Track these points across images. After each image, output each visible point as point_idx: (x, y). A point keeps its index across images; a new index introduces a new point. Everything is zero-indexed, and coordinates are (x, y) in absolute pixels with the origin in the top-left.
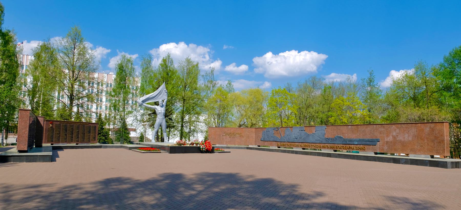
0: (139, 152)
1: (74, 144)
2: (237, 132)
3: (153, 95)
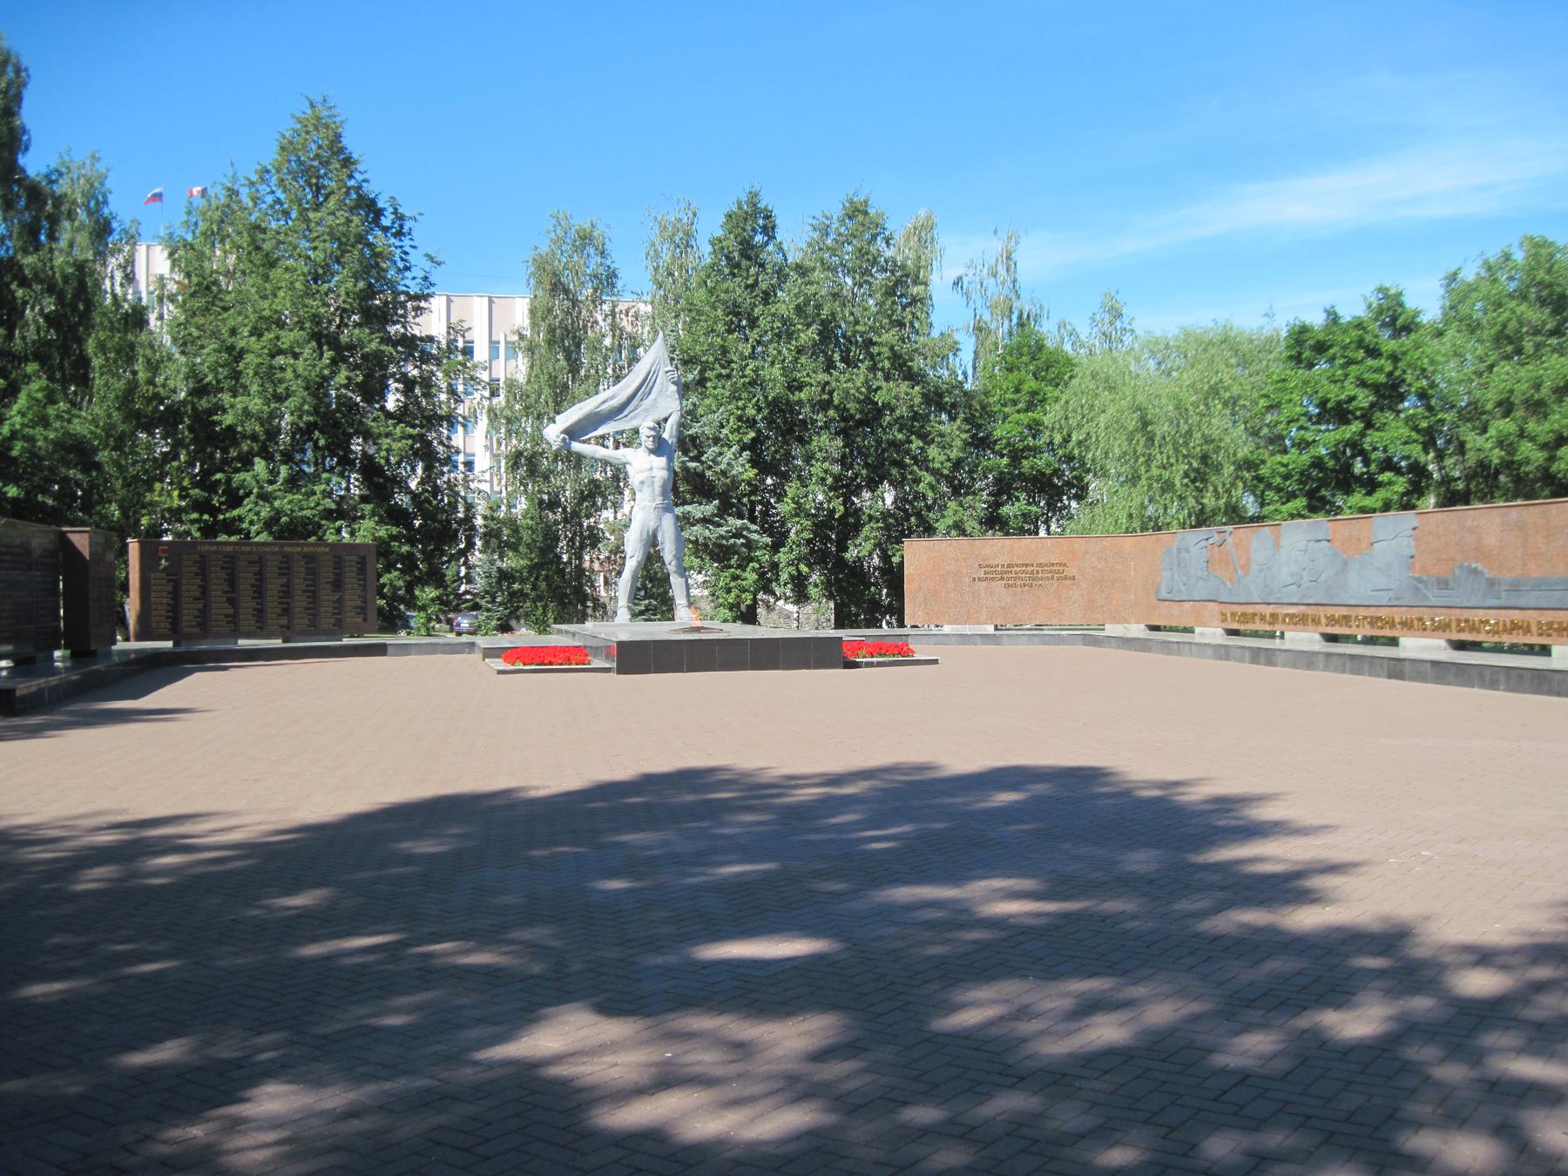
0: (1171, 629)
1: (277, 643)
2: (1042, 561)
3: (613, 397)
